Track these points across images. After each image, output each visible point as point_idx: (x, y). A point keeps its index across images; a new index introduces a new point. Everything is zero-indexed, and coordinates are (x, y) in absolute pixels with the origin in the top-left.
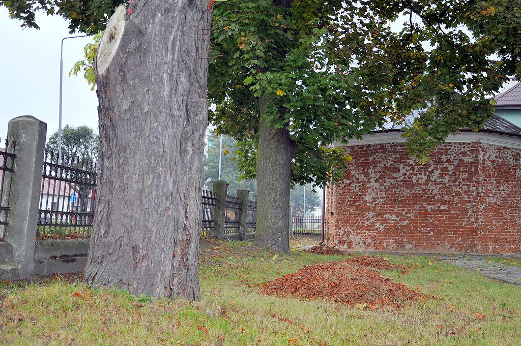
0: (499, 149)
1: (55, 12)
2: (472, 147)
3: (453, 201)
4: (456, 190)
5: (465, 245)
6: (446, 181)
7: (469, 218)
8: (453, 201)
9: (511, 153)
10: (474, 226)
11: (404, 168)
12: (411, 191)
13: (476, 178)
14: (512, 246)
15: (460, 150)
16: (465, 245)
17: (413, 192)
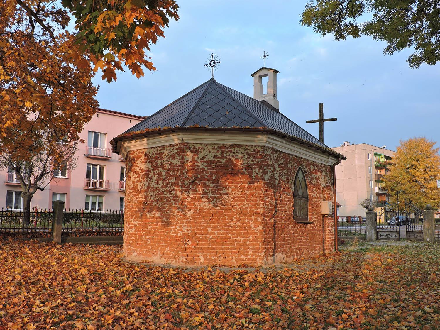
0: (222, 148)
1: (140, 65)
2: (179, 148)
3: (164, 208)
4: (166, 196)
5: (171, 255)
6: (160, 186)
7: (175, 226)
8: (164, 208)
9: (243, 151)
10: (179, 235)
11: (133, 175)
12: (137, 198)
13: (181, 182)
14: (243, 257)
15: (171, 152)
16: (171, 255)
17: (138, 199)
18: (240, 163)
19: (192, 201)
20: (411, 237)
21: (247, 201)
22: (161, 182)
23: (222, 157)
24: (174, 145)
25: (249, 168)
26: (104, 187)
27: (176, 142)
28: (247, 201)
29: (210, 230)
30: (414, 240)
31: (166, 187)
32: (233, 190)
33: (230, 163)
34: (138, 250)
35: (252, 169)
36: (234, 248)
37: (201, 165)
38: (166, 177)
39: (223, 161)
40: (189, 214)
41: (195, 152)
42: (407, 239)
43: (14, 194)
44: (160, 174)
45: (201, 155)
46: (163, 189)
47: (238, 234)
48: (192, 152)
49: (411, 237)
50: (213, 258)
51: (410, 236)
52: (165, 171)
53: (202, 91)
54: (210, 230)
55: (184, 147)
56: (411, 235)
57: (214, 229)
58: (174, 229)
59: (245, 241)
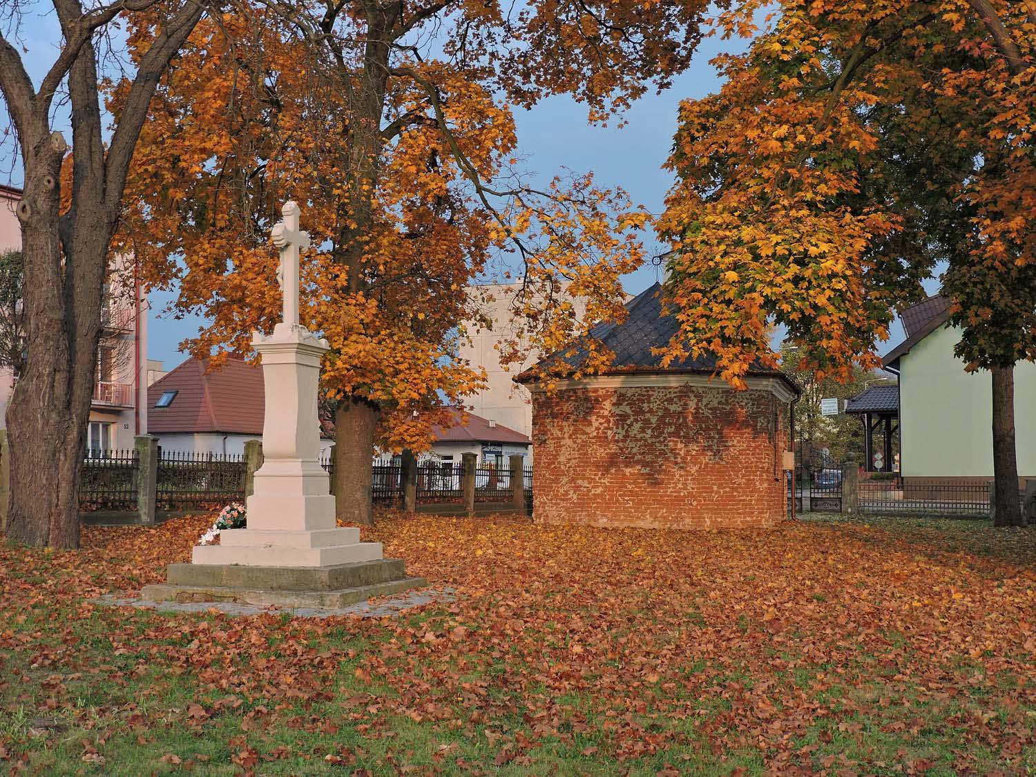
7: (675, 483)
14: (748, 519)
18: (742, 412)
19: (697, 455)
20: (818, 508)
21: (753, 454)
22: (649, 431)
23: (727, 403)
24: (671, 388)
25: (754, 416)
26: (113, 402)
27: (673, 385)
28: (753, 454)
29: (715, 488)
30: (825, 511)
31: (658, 437)
32: (739, 442)
33: (732, 412)
34: (610, 515)
35: (757, 417)
36: (739, 509)
37: (707, 412)
38: (658, 425)
39: (728, 408)
40: (694, 469)
41: (699, 397)
42: (812, 510)
43: (101, 426)
44: (647, 421)
45: (705, 401)
46: (654, 440)
47: (744, 492)
48: (695, 396)
49: (818, 508)
50: (719, 520)
51: (816, 506)
52: (656, 418)
53: (638, 300)
54: (715, 488)
55: (685, 392)
56: (819, 503)
57: (720, 486)
58: (674, 488)
59: (751, 500)
